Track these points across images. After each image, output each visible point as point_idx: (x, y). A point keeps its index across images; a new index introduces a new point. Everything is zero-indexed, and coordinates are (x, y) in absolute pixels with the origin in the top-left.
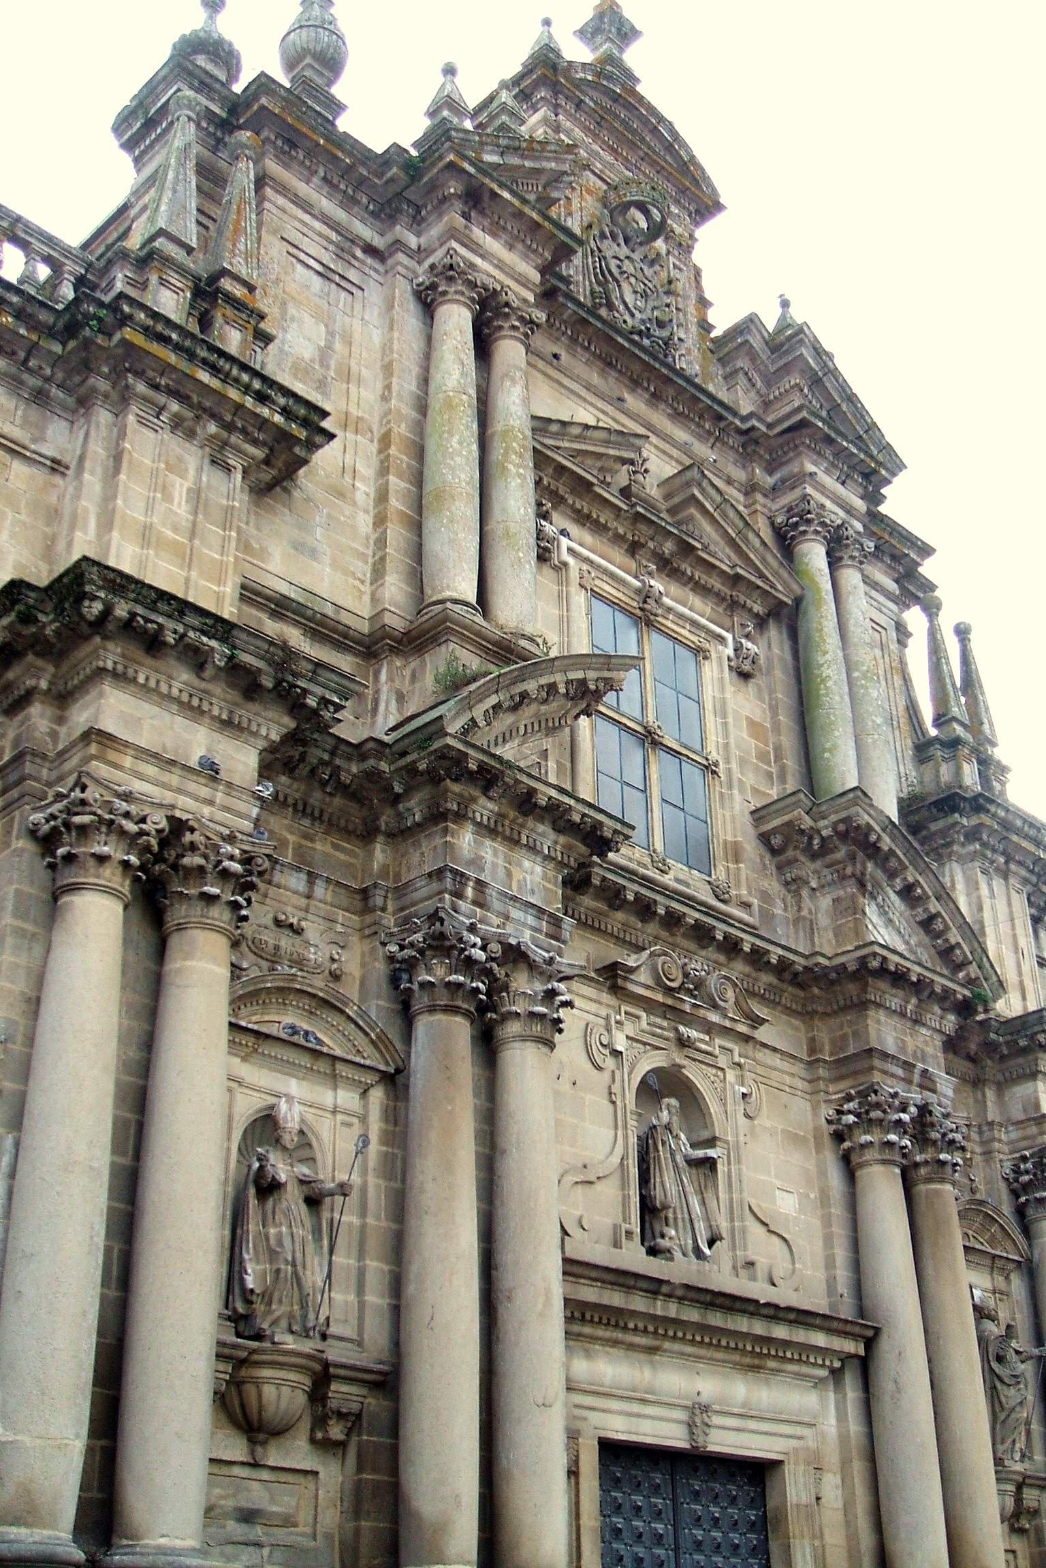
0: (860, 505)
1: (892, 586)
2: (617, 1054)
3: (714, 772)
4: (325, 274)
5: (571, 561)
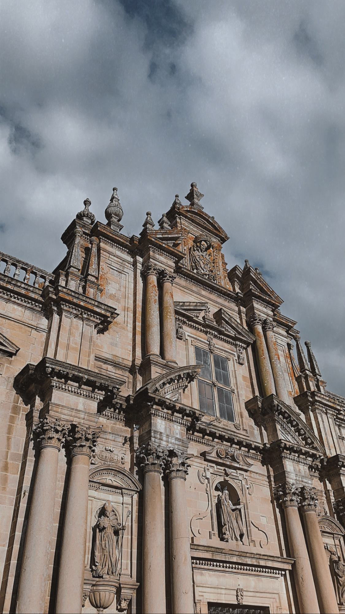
0: (271, 313)
1: (285, 334)
2: (208, 479)
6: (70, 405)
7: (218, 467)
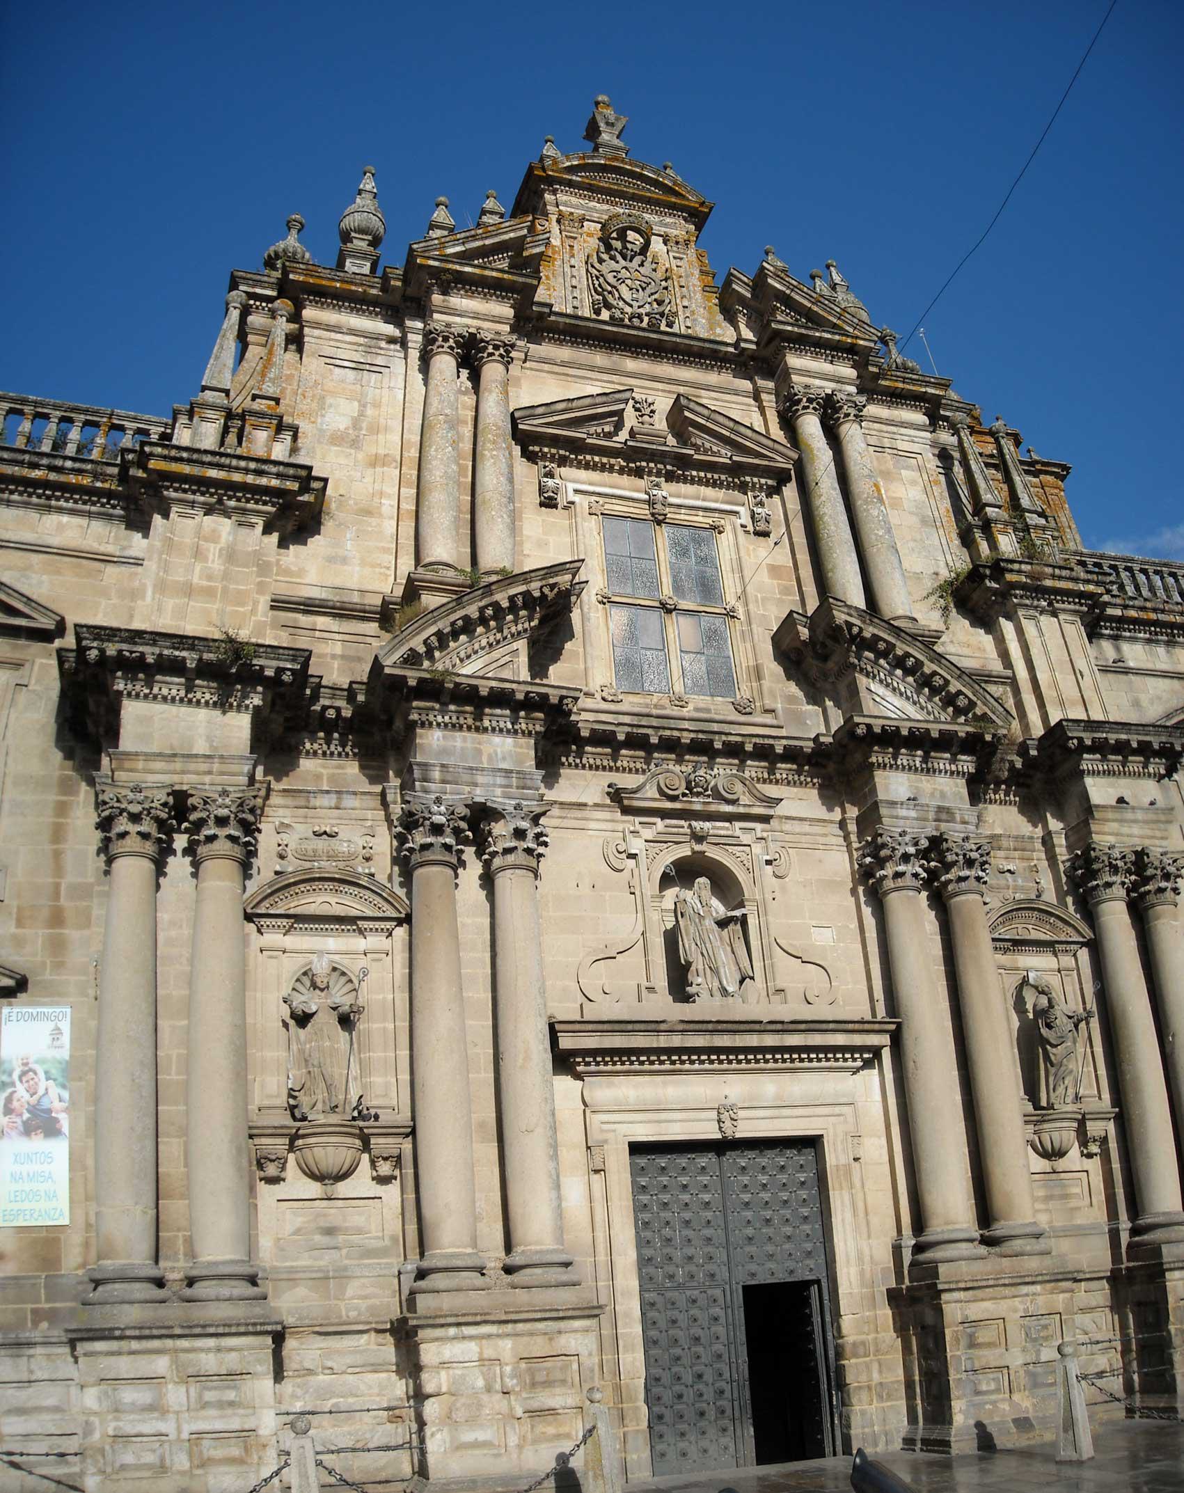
3: (733, 617)
4: (358, 367)
5: (577, 498)
6: (181, 737)
7: (668, 821)
